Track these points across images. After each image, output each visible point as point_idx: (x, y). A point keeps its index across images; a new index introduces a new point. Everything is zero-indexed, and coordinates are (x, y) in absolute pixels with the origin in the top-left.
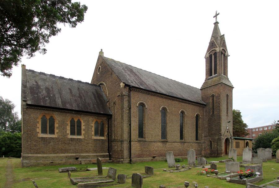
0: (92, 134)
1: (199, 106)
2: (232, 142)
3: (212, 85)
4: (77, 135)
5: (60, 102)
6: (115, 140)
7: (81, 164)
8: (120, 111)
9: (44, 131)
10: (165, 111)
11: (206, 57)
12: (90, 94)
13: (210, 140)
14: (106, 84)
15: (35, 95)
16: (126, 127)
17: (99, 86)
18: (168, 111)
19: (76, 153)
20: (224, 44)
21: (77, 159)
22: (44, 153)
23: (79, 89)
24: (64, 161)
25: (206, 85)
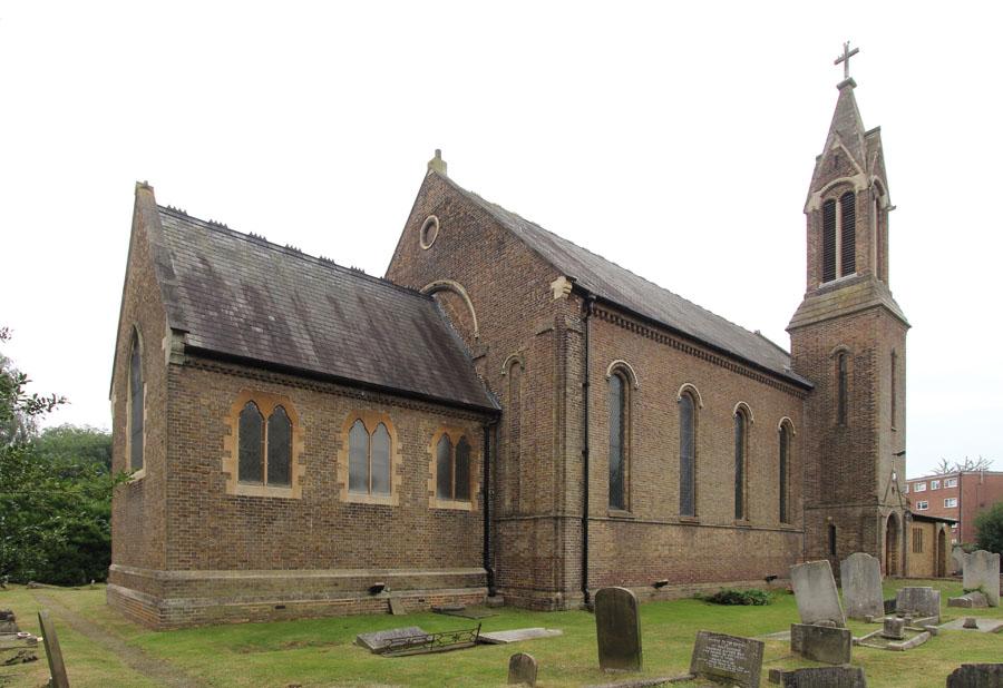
0: (430, 489)
1: (791, 394)
2: (905, 528)
3: (840, 313)
4: (273, 480)
5: (311, 348)
7: (391, 612)
8: (552, 395)
9: (249, 471)
10: (689, 404)
12: (405, 324)
13: (827, 521)
15: (211, 313)
16: (560, 459)
17: (429, 296)
18: (702, 404)
19: (369, 565)
21: (376, 590)
22: (249, 564)
23: (361, 301)
24: (327, 600)
25: (809, 315)
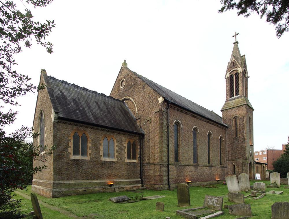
3: (235, 106)
6: (149, 164)
9: (75, 152)
11: (227, 77)
14: (133, 99)
20: (244, 66)
22: (76, 179)
23: (104, 103)
24: (97, 188)
25: (227, 106)
